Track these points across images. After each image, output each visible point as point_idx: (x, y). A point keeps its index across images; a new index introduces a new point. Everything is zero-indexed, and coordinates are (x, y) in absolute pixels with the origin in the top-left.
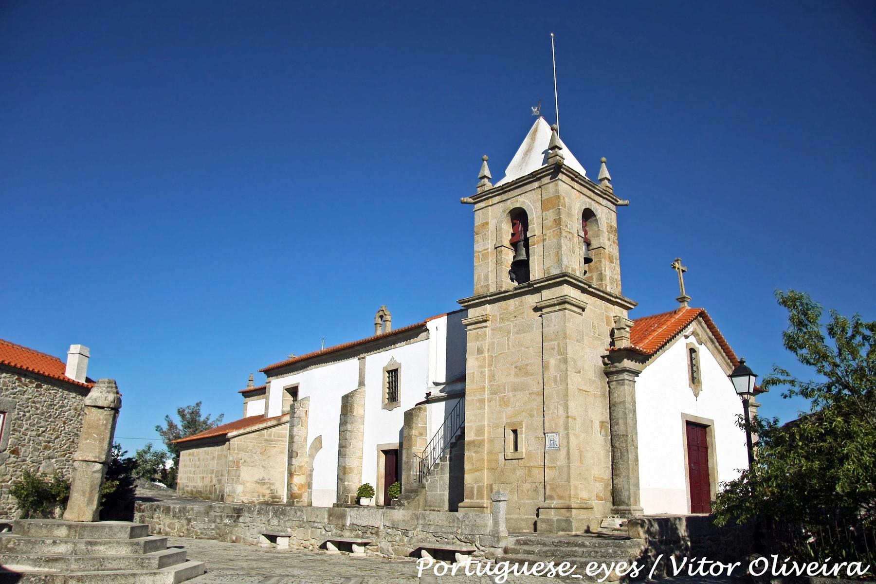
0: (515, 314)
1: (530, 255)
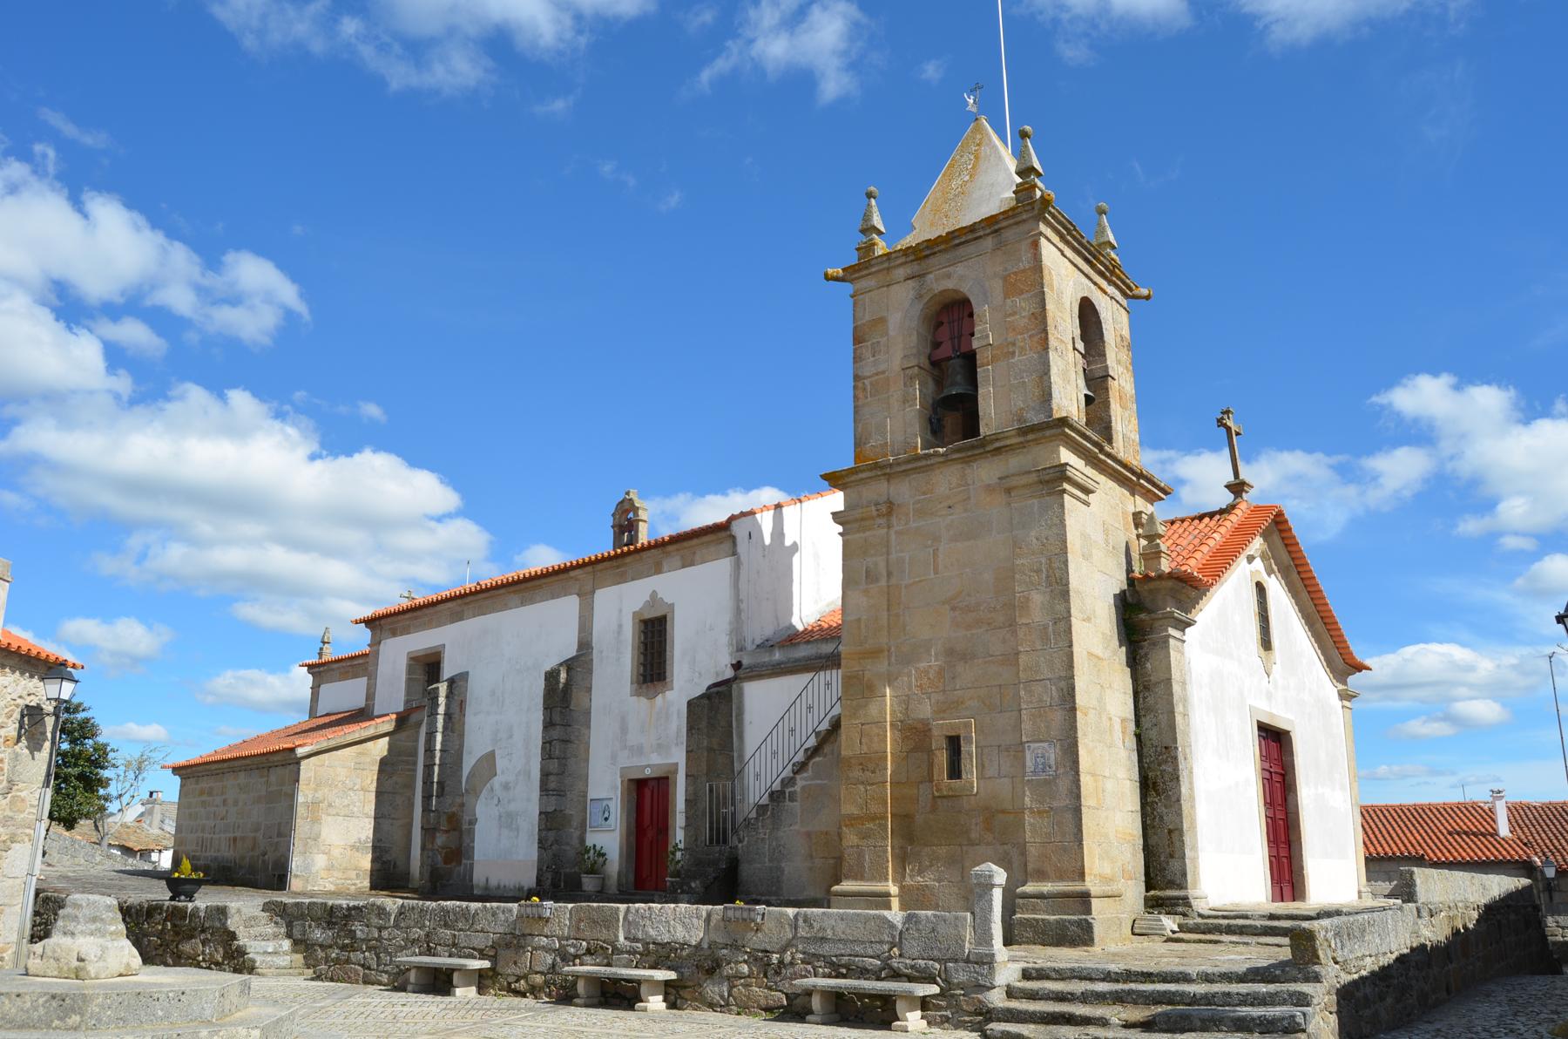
0: (950, 502)
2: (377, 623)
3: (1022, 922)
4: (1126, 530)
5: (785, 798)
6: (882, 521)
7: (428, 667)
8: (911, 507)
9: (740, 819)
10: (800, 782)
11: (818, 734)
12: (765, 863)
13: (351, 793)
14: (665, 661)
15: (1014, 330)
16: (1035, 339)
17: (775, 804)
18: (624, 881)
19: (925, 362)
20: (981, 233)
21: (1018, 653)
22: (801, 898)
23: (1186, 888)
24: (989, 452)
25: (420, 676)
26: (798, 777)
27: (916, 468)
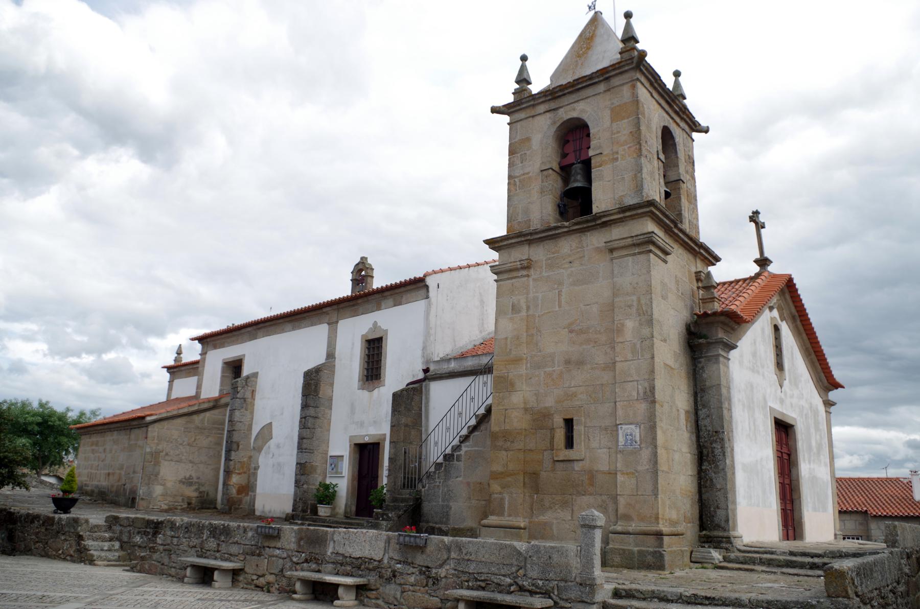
0: (570, 259)
1: (593, 181)
2: (205, 340)
3: (612, 550)
4: (691, 283)
5: (454, 459)
7: (235, 367)
8: (544, 262)
9: (424, 472)
10: (464, 449)
11: (477, 416)
12: (439, 502)
13: (181, 447)
14: (380, 367)
15: (618, 143)
16: (633, 149)
17: (447, 463)
18: (349, 510)
19: (556, 166)
20: (597, 80)
21: (615, 363)
22: (462, 527)
23: (729, 531)
24: (598, 224)
25: (229, 374)
26: (463, 445)
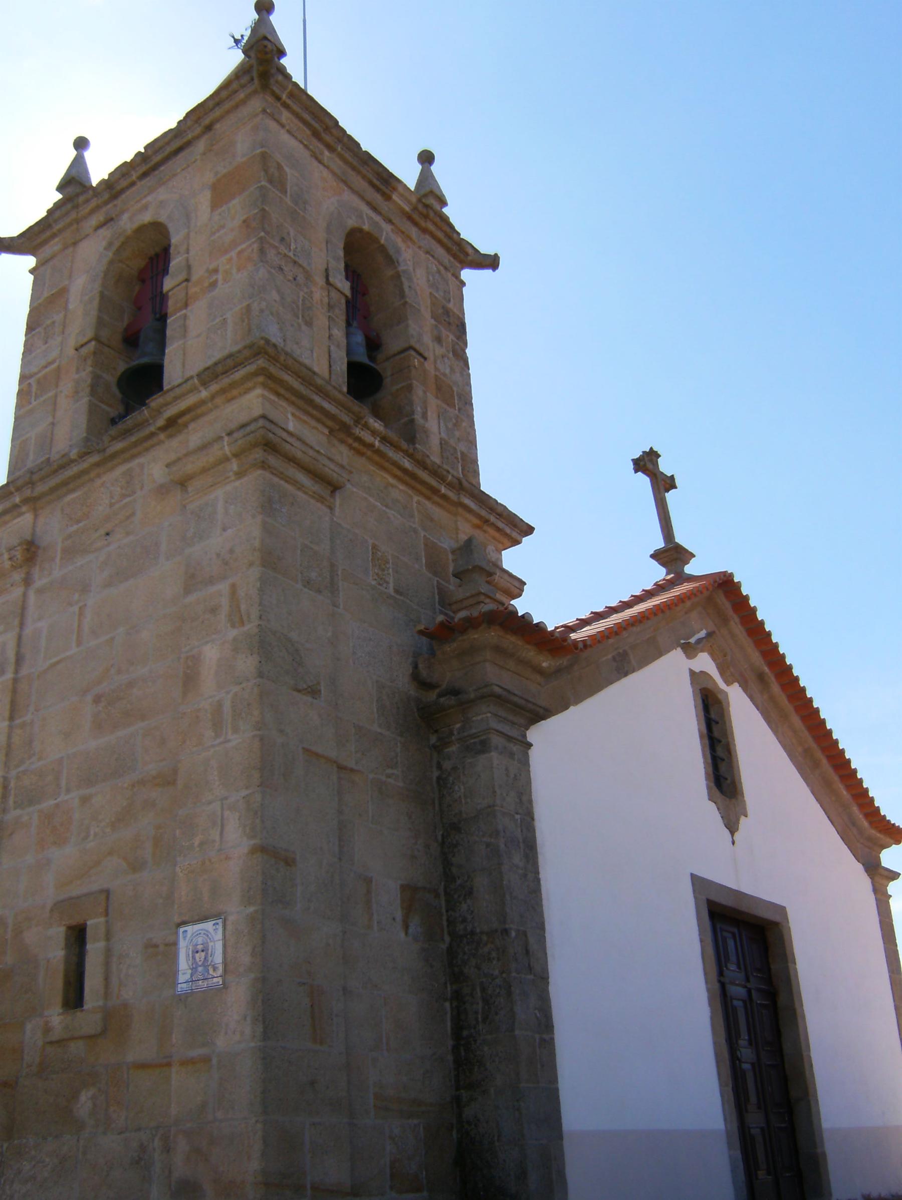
6: (17, 576)
27: (65, 483)
